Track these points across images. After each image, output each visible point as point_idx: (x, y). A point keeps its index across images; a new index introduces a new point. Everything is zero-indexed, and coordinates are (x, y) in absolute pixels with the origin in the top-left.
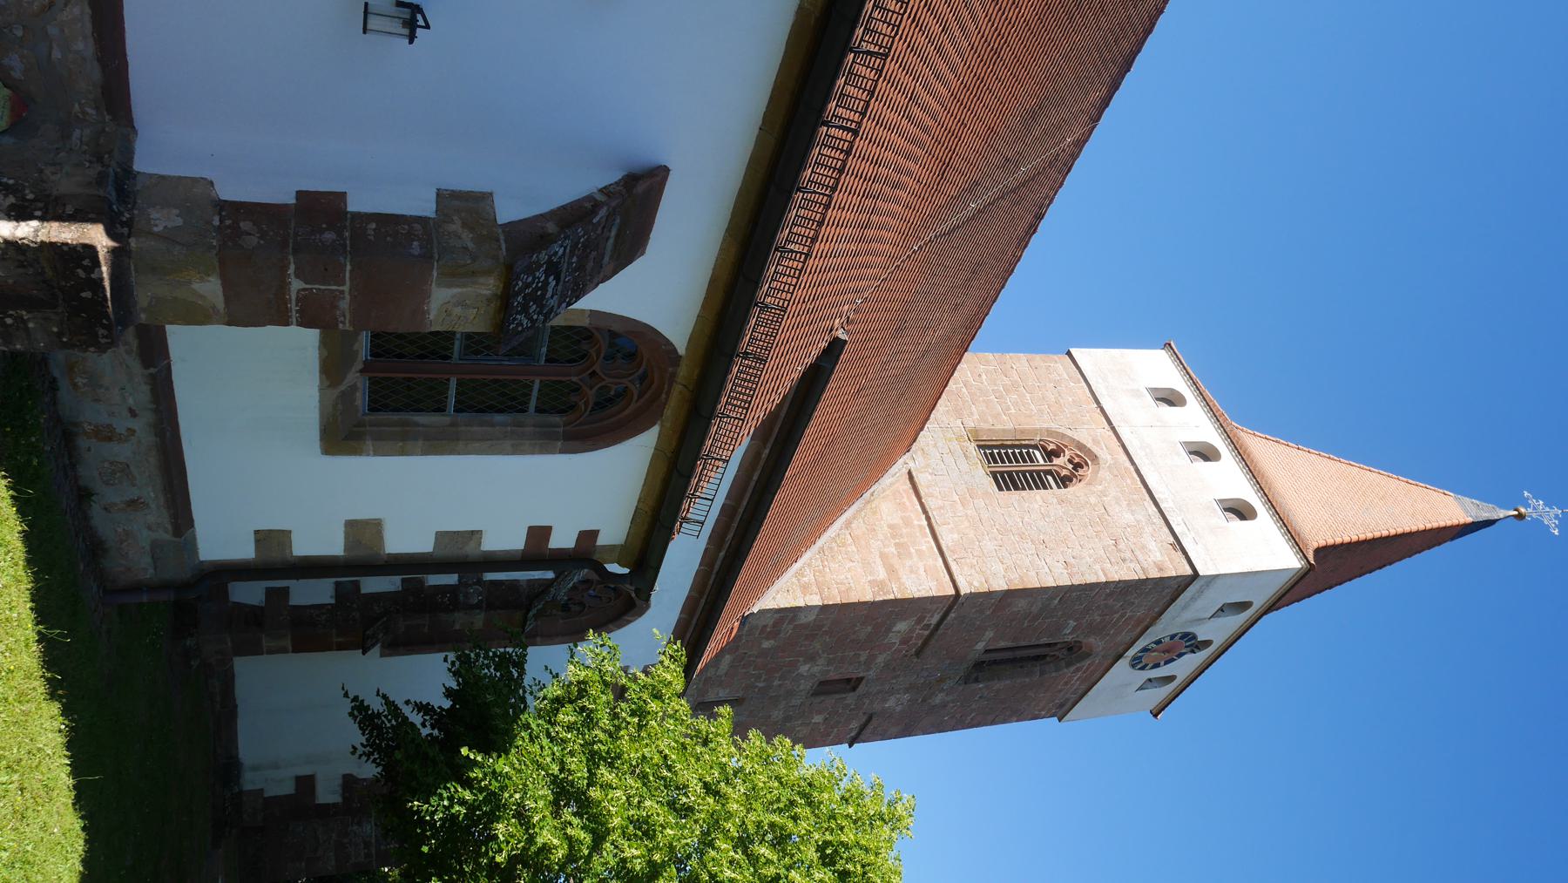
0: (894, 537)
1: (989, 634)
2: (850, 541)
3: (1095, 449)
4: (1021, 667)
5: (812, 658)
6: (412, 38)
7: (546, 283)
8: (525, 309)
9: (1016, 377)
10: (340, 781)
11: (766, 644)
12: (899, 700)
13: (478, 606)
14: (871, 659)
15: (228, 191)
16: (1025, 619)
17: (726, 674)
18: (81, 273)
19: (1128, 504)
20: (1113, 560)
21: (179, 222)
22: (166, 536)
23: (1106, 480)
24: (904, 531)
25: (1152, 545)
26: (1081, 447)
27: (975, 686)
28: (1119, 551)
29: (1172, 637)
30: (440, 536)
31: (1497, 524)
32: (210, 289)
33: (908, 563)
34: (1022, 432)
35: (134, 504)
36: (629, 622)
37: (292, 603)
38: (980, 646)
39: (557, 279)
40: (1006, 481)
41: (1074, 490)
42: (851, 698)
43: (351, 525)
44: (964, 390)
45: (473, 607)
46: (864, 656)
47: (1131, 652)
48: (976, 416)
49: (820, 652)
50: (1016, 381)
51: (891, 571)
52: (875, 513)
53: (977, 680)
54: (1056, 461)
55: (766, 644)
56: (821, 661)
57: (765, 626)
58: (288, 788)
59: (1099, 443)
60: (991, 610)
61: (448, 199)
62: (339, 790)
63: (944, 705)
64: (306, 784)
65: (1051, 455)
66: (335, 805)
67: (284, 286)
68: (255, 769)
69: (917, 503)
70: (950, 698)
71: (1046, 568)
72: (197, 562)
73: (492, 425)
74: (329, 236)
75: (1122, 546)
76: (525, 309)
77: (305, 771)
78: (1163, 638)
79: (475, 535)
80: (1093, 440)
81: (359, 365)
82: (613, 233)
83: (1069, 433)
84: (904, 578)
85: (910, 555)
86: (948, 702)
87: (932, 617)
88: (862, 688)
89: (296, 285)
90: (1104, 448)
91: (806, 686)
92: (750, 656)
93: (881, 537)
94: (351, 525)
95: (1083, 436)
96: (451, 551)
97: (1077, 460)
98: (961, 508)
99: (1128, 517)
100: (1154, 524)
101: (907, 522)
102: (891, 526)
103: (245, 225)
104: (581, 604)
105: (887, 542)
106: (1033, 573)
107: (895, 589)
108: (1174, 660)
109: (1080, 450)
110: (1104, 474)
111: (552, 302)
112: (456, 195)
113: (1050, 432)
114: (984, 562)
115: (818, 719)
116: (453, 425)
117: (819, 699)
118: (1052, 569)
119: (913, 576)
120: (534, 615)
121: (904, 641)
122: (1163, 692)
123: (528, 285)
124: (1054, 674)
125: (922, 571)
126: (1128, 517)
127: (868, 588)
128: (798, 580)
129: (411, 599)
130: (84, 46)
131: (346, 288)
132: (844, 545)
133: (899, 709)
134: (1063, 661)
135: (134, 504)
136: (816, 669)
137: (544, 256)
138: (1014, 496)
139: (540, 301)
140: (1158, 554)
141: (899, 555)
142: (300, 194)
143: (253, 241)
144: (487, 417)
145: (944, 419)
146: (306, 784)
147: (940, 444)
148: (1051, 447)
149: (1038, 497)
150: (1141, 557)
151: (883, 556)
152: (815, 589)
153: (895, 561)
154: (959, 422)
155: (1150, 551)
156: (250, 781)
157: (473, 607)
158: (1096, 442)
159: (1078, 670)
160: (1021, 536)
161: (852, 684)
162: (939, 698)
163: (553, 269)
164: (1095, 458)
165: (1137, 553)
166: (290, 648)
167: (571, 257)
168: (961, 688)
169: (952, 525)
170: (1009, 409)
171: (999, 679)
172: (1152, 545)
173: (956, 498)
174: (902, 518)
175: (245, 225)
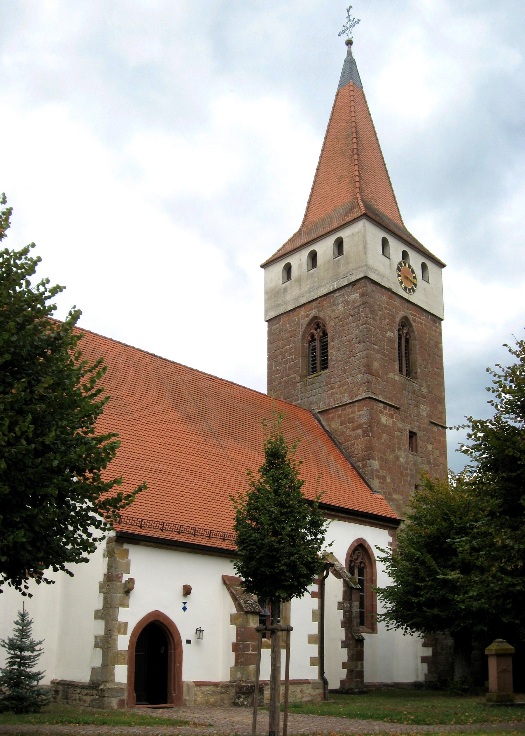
0: (345, 424)
1: (391, 375)
2: (346, 443)
3: (310, 317)
4: (411, 350)
5: (397, 458)
6: (203, 631)
7: (249, 603)
8: (254, 608)
9: (278, 351)
10: (424, 648)
11: (389, 480)
12: (423, 410)
13: (351, 604)
14: (400, 430)
15: (233, 664)
16: (384, 359)
17: (402, 495)
18: (250, 688)
19: (335, 306)
20: (358, 319)
21: (239, 672)
22: (310, 686)
23: (324, 315)
24: (343, 418)
25: (353, 297)
26: (309, 324)
27: (419, 374)
28: (354, 315)
29: (399, 276)
30: (313, 620)
31: (355, 56)
32: (252, 667)
33: (356, 419)
34: (303, 353)
35: (302, 691)
36: (368, 545)
37: (347, 661)
38: (397, 378)
39: (248, 601)
40: (325, 365)
41: (329, 330)
42: (420, 434)
43: (309, 642)
44: (284, 379)
45: (351, 605)
46: (397, 434)
47: (406, 295)
48: (296, 375)
49: (394, 455)
50: (280, 352)
51: (359, 427)
52: (336, 431)
53: (416, 373)
54: (316, 336)
55: (389, 480)
56: (399, 453)
57: (380, 483)
58: (425, 666)
59: (307, 314)
60: (378, 378)
61: (232, 623)
62: (427, 648)
63: (428, 386)
64: (424, 659)
65: (313, 339)
66: (433, 650)
67: (251, 654)
68: (417, 677)
69: (332, 410)
70: (424, 384)
71: (360, 353)
72: (320, 681)
73: (283, 609)
74: (241, 646)
75: (352, 313)
76: (254, 608)
77: (419, 660)
78: (399, 281)
79: (313, 612)
80: (306, 317)
81: (268, 640)
82: (237, 588)
83: (303, 329)
84: (362, 421)
85: (353, 417)
86: (427, 384)
87: (380, 407)
88: (414, 430)
89: (250, 652)
90: (310, 312)
91: (411, 458)
92: (394, 486)
93: (345, 430)
94: (309, 642)
95: (305, 321)
96: (318, 617)
97: (316, 326)
98: (335, 390)
99: (340, 307)
100: (343, 294)
101: (340, 416)
102: (341, 425)
103: (239, 661)
104: (361, 563)
105: (348, 427)
106: (362, 360)
107: (366, 426)
108: (412, 269)
109: (311, 324)
110: (321, 315)
111: (252, 601)
112: (231, 621)
113: (303, 339)
114: (357, 383)
115: (430, 447)
116: (283, 618)
117: (419, 449)
118: (361, 350)
119: (361, 417)
120: (355, 585)
121: (392, 416)
122: (430, 265)
123: (249, 608)
124: (416, 333)
125: (359, 413)
126: (340, 307)
127: (365, 439)
128: (361, 468)
129: (347, 625)
130: (208, 688)
131: (251, 643)
132: (348, 446)
133: (428, 409)
134: (410, 329)
135: (302, 691)
136: (403, 455)
137: (244, 605)
138: (330, 363)
139: (252, 604)
140: (357, 295)
141: (353, 422)
142: (233, 651)
143: (243, 660)
144: (281, 610)
145: (297, 391)
146: (424, 659)
147: (307, 396)
148: (310, 338)
149: (331, 351)
150: (358, 304)
151: (353, 430)
152: (364, 462)
153: (356, 424)
154: (298, 384)
155: (355, 298)
156: (421, 678)
157: (351, 605)
158: (307, 316)
159: (414, 321)
160: (347, 362)
161: (412, 435)
162: (424, 390)
163: (245, 602)
164: (315, 318)
165: (356, 305)
166: (362, 662)
167: (242, 598)
168: (419, 380)
169: (341, 396)
170: (292, 358)
171: (416, 362)
172: (353, 297)
173: (330, 392)
174: (338, 418)
175: (239, 661)
